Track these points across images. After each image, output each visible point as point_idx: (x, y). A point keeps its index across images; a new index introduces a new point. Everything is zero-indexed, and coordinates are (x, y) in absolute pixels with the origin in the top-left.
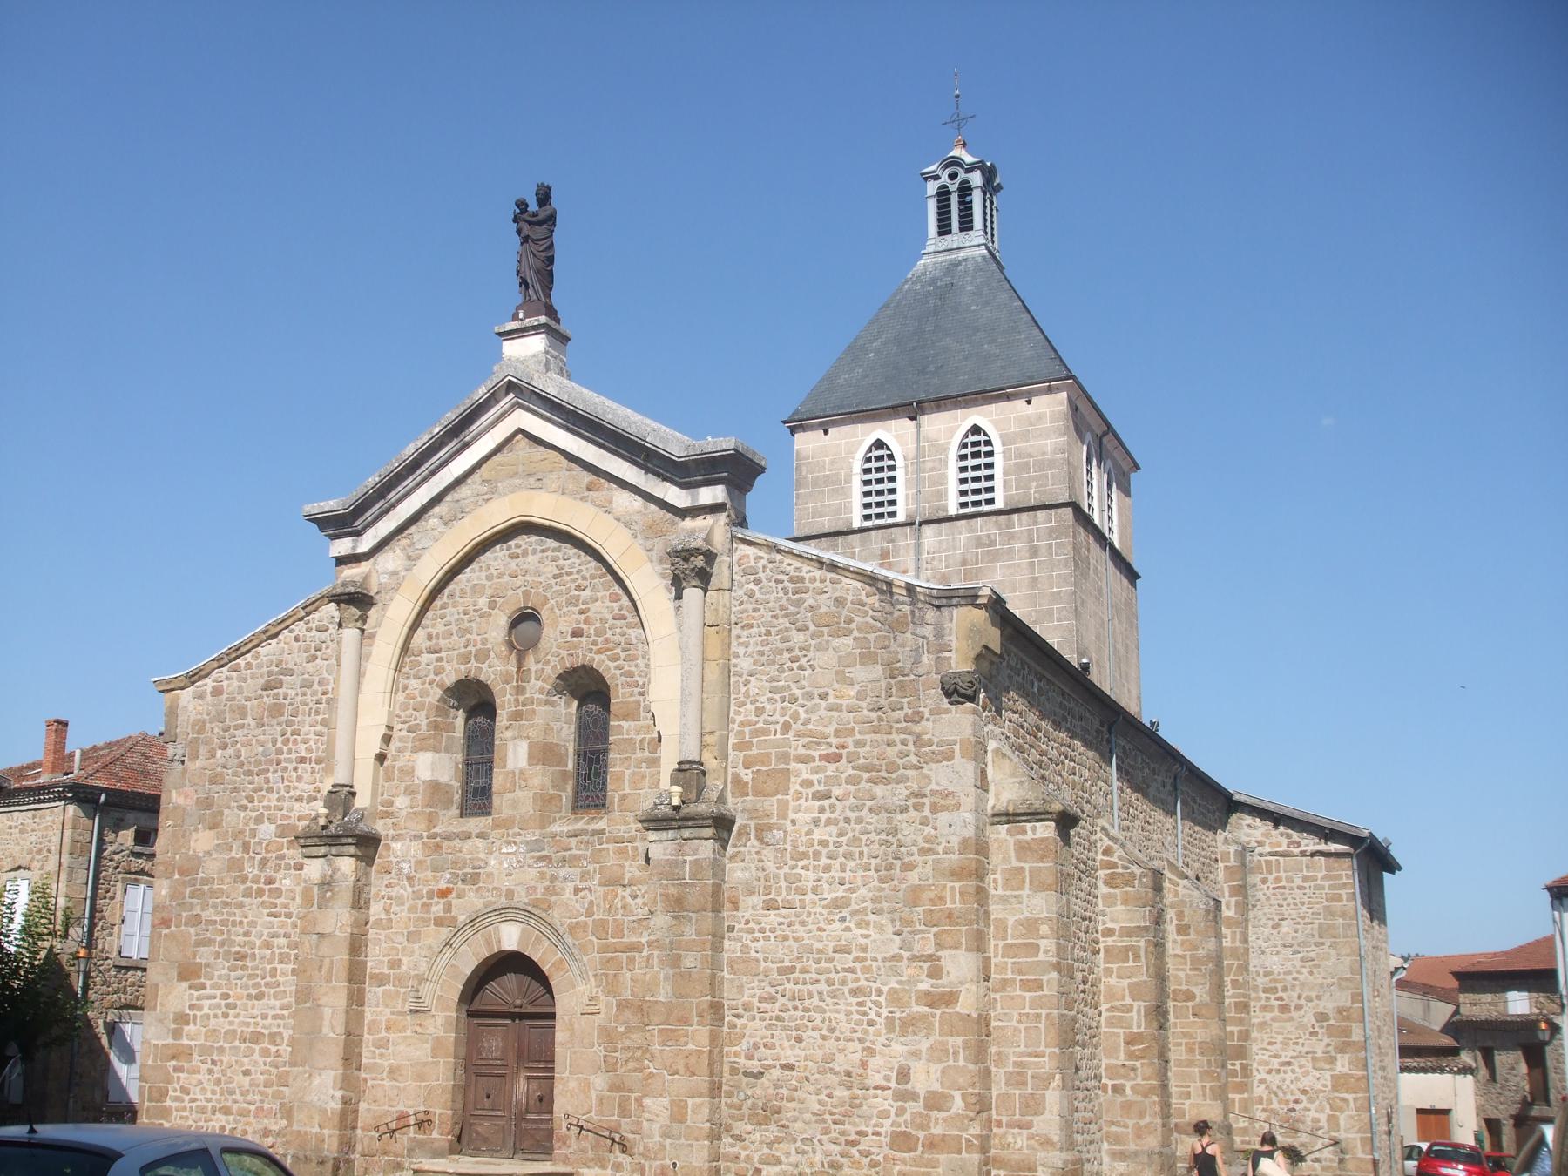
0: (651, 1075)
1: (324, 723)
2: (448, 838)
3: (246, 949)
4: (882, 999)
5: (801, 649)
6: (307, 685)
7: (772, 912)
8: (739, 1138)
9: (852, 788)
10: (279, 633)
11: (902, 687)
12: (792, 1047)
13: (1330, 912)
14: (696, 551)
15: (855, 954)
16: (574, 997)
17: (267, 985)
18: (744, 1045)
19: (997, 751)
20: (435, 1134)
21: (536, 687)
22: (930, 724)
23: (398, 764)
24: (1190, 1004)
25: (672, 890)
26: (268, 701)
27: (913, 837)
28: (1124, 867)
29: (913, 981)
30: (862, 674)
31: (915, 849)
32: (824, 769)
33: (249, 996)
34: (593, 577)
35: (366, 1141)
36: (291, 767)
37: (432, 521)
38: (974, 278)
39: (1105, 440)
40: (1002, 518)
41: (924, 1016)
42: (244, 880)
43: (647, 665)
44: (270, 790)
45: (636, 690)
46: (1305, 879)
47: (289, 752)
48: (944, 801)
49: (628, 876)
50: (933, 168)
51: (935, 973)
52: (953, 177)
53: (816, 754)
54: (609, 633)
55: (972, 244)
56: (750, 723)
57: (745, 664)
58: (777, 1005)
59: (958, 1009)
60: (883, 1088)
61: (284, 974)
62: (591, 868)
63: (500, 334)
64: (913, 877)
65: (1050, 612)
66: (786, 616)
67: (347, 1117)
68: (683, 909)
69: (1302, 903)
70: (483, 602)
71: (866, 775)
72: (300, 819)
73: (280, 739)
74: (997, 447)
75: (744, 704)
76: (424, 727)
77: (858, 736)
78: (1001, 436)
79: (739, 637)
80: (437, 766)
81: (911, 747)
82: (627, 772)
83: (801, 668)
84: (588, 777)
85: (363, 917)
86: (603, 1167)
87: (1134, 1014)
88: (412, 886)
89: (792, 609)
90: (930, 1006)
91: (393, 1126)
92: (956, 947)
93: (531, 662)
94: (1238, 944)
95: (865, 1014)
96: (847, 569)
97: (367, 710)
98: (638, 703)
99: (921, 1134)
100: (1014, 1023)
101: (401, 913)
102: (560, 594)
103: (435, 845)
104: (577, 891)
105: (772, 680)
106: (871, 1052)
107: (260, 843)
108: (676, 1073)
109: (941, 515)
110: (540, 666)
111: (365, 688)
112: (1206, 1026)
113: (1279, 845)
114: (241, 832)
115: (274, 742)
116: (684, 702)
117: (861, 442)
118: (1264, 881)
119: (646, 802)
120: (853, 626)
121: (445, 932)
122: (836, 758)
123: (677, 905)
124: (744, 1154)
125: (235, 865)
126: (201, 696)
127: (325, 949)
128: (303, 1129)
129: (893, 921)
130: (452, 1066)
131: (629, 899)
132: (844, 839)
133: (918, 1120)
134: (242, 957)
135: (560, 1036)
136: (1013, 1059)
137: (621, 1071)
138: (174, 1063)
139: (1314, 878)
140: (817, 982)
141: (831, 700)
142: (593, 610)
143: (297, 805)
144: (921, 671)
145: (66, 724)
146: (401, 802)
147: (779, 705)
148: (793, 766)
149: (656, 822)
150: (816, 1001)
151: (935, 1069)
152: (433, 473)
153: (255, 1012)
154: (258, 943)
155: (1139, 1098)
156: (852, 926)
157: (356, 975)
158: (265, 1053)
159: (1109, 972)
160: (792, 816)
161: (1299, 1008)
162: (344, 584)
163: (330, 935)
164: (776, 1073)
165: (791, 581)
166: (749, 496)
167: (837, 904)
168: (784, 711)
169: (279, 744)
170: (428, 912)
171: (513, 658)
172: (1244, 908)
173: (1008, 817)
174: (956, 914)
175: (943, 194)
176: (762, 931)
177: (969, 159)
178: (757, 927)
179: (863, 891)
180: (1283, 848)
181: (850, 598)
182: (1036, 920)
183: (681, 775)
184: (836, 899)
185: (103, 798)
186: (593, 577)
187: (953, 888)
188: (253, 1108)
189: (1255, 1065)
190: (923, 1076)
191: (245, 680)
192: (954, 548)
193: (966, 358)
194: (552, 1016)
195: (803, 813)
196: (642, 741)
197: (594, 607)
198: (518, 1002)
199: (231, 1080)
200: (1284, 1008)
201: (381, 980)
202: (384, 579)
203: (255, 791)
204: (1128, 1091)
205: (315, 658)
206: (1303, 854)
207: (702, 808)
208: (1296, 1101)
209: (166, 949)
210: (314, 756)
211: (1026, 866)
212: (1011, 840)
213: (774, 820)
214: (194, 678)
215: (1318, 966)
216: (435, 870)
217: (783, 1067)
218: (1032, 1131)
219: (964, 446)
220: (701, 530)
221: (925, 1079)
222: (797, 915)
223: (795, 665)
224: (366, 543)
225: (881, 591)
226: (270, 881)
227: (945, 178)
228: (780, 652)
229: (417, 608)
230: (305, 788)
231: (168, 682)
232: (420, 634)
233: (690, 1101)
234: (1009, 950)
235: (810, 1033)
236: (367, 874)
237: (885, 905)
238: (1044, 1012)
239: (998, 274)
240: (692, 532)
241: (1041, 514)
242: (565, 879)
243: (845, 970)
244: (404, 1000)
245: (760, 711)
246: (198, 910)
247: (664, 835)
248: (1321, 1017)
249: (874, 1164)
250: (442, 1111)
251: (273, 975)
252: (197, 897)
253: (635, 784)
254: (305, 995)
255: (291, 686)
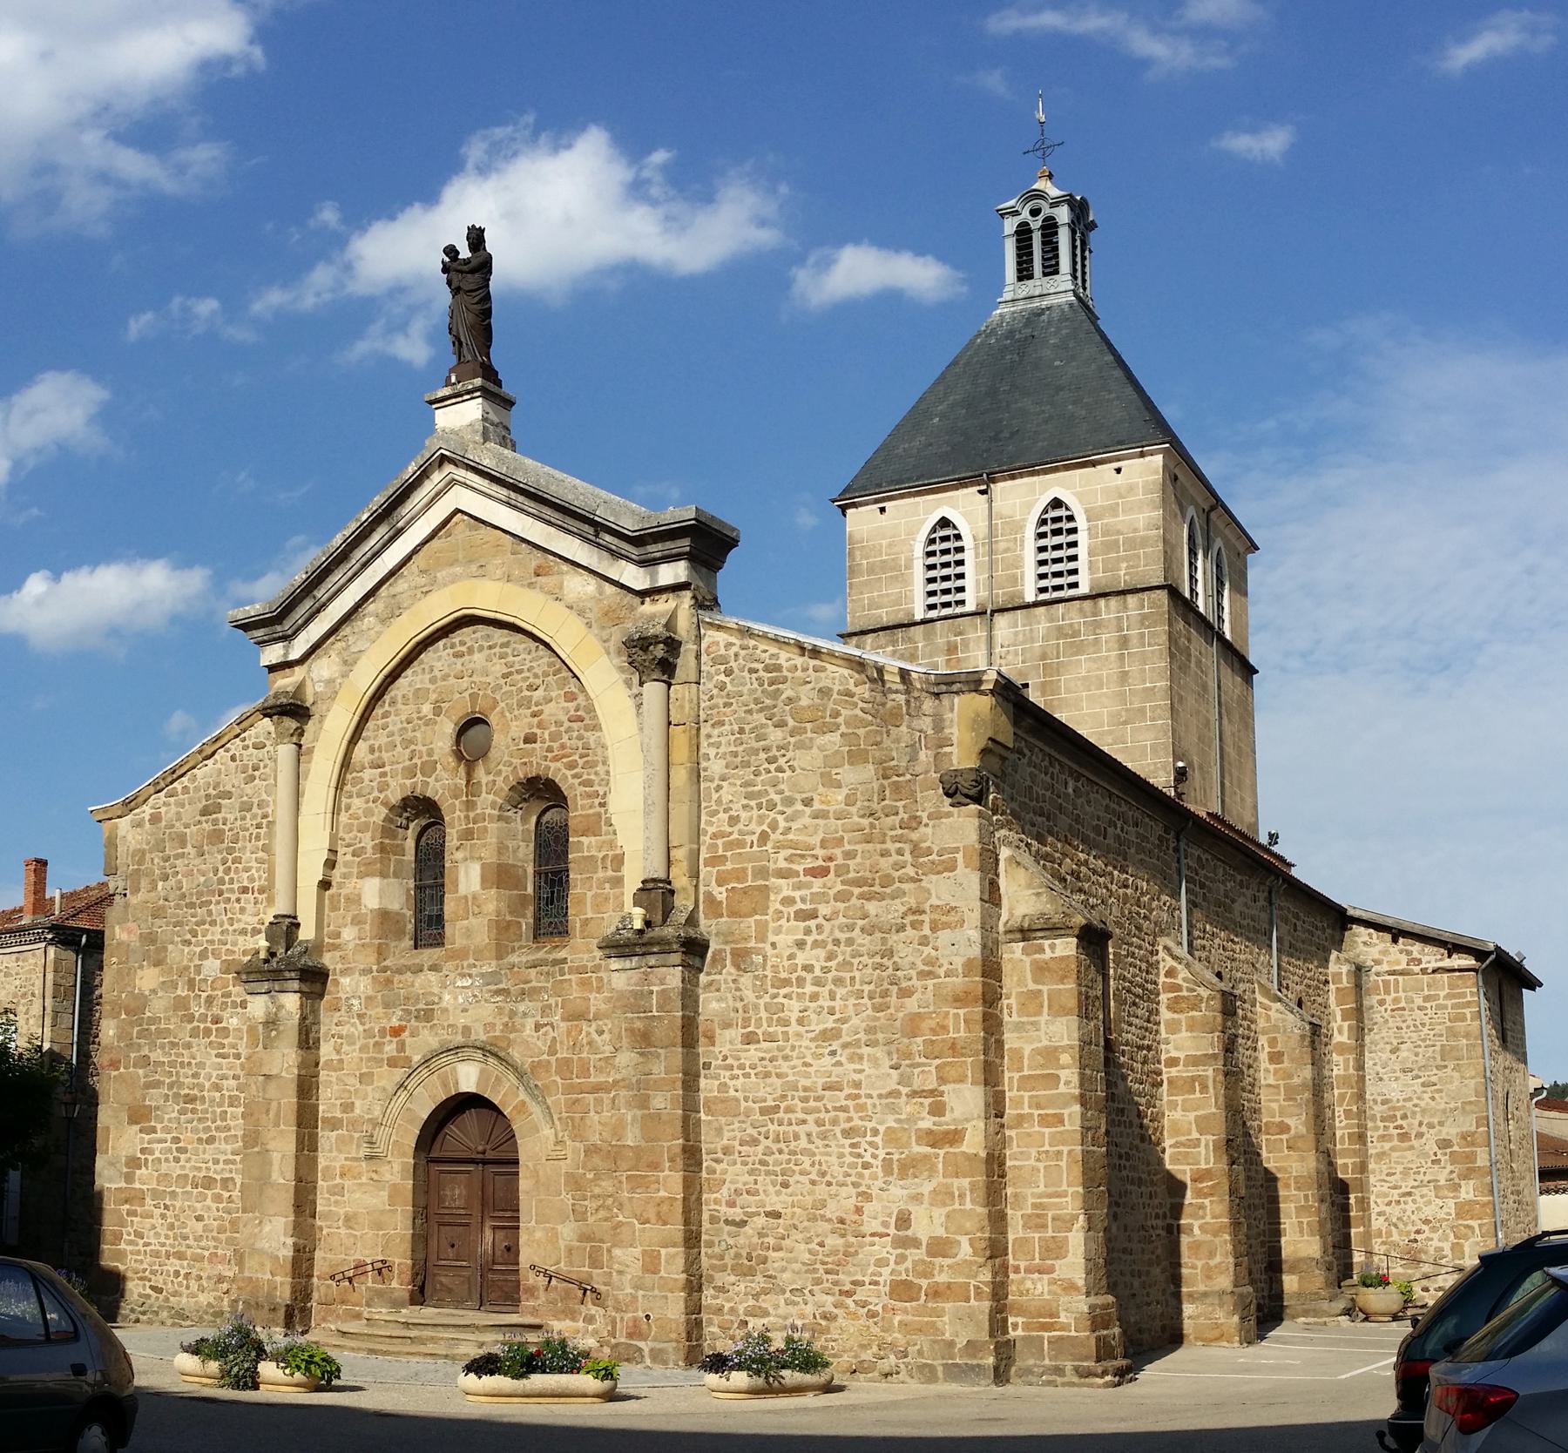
0: (620, 1224)
1: (265, 849)
2: (400, 971)
3: (195, 1092)
4: (878, 1140)
5: (779, 748)
6: (246, 808)
7: (752, 1047)
8: (722, 1289)
9: (841, 906)
10: (213, 754)
11: (897, 787)
12: (778, 1193)
13: (1452, 1033)
14: (655, 640)
15: (847, 1091)
16: (539, 1144)
17: (217, 1129)
18: (724, 1191)
19: (1011, 859)
20: (395, 1284)
21: (487, 802)
22: (929, 830)
23: (344, 892)
24: (1284, 1137)
25: (638, 1024)
26: (207, 827)
27: (910, 959)
28: (1189, 990)
29: (912, 1119)
30: (849, 775)
31: (913, 973)
32: (809, 886)
33: (200, 1140)
34: (546, 674)
35: (323, 1289)
36: (233, 898)
37: (367, 621)
38: (1059, 329)
39: (1213, 515)
40: (1087, 604)
41: (926, 1157)
42: (191, 1019)
43: (608, 773)
44: (213, 923)
45: (597, 801)
46: (1427, 999)
47: (232, 880)
48: (946, 918)
49: (593, 1009)
50: (1012, 203)
51: (938, 1110)
52: (1035, 212)
53: (800, 868)
54: (565, 737)
55: (1059, 289)
56: (722, 835)
57: (715, 767)
58: (760, 1148)
59: (964, 1148)
60: (881, 1236)
61: (234, 1117)
62: (552, 1001)
63: (431, 402)
64: (912, 1004)
65: (1142, 711)
66: (761, 710)
67: (302, 1263)
68: (650, 1045)
69: (1423, 1025)
70: (427, 709)
71: (857, 891)
72: (245, 953)
73: (221, 869)
74: (1081, 522)
75: (716, 813)
76: (369, 850)
77: (847, 847)
78: (1086, 511)
79: (709, 736)
80: (381, 893)
81: (908, 857)
82: (589, 894)
83: (780, 770)
84: (550, 901)
85: (312, 1057)
86: (573, 1319)
87: (1202, 1149)
88: (363, 1024)
89: (768, 702)
90: (933, 1146)
91: (351, 1274)
92: (961, 1080)
93: (481, 774)
94: (1351, 1071)
95: (859, 1156)
96: (831, 654)
97: (304, 833)
98: (599, 815)
99: (924, 1283)
100: (1032, 1162)
101: (352, 1054)
102: (509, 694)
103: (385, 978)
104: (538, 1027)
105: (746, 784)
106: (867, 1197)
107: (205, 980)
108: (647, 1221)
109: (1017, 602)
110: (491, 777)
111: (304, 809)
112: (1302, 1159)
113: (1398, 963)
114: (187, 968)
115: (216, 871)
116: (647, 813)
117: (924, 521)
118: (1382, 1002)
119: (609, 925)
120: (840, 720)
121: (399, 1074)
122: (824, 872)
123: (644, 1040)
124: (727, 1306)
125: (181, 1004)
126: (138, 824)
127: (272, 1091)
128: (254, 1276)
129: (889, 1053)
130: (410, 1215)
131: (595, 1036)
132: (833, 964)
133: (920, 1268)
134: (192, 1100)
135: (524, 1184)
136: (1031, 1200)
137: (591, 1220)
138: (127, 1206)
139: (1436, 997)
140: (804, 1122)
141: (817, 805)
142: (546, 712)
143: (241, 939)
144: (918, 769)
145: (45, 863)
146: (349, 934)
147: (755, 812)
148: (774, 881)
149: (619, 947)
150: (803, 1143)
151: (939, 1213)
152: (365, 565)
153: (207, 1156)
154: (207, 1085)
155: (1209, 1237)
156: (843, 1059)
157: (307, 1120)
158: (218, 1198)
159: (1173, 1105)
160: (772, 938)
161: (1420, 1135)
162: (276, 696)
163: (277, 1076)
164: (761, 1221)
165: (767, 669)
166: (720, 574)
167: (826, 1036)
168: (761, 820)
169: (220, 874)
170: (381, 1052)
171: (462, 770)
172: (1360, 1032)
173: (1025, 933)
174: (960, 1044)
175: (1023, 233)
176: (741, 1067)
177: (1053, 192)
178: (735, 1064)
179: (855, 1021)
180: (1403, 966)
181: (836, 688)
182: (1056, 1048)
183: (644, 895)
184: (825, 1030)
185: (84, 940)
186: (546, 674)
187: (957, 1016)
188: (207, 1253)
189: (1373, 1198)
190: (926, 1221)
191: (183, 805)
192: (1032, 640)
193: (1046, 422)
194: (516, 1162)
195: (785, 935)
196: (604, 858)
197: (548, 709)
198: (480, 1148)
199: (184, 1225)
200: (1404, 1137)
201: (334, 1124)
202: (320, 688)
203: (197, 924)
204: (1196, 1231)
205: (253, 778)
206: (1424, 971)
207: (668, 931)
208: (1418, 1232)
209: (116, 1091)
210: (256, 884)
211: (1045, 988)
212: (1027, 960)
213: (752, 944)
214: (129, 805)
215: (1440, 1091)
216: (387, 1006)
217: (768, 1214)
218: (1054, 1275)
219: (1043, 522)
220: (662, 615)
221: (927, 1225)
222: (779, 1049)
223: (772, 767)
224: (299, 648)
225: (872, 680)
226: (217, 1020)
227: (1025, 215)
228: (756, 752)
229: (356, 718)
230: (249, 920)
231: (105, 810)
232: (361, 748)
233: (663, 1251)
234: (1026, 1083)
235: (797, 1177)
236: (315, 1012)
237: (880, 1036)
238: (1065, 1149)
239: (1087, 325)
240: (652, 617)
241: (1132, 600)
242: (525, 1014)
243: (835, 1109)
244: (358, 1146)
245: (734, 820)
246: (145, 1051)
247: (627, 963)
248: (1444, 1144)
249: (872, 1315)
250: (401, 1259)
251: (224, 1119)
252: (145, 1037)
253: (597, 908)
254: (252, 1138)
255: (229, 812)
